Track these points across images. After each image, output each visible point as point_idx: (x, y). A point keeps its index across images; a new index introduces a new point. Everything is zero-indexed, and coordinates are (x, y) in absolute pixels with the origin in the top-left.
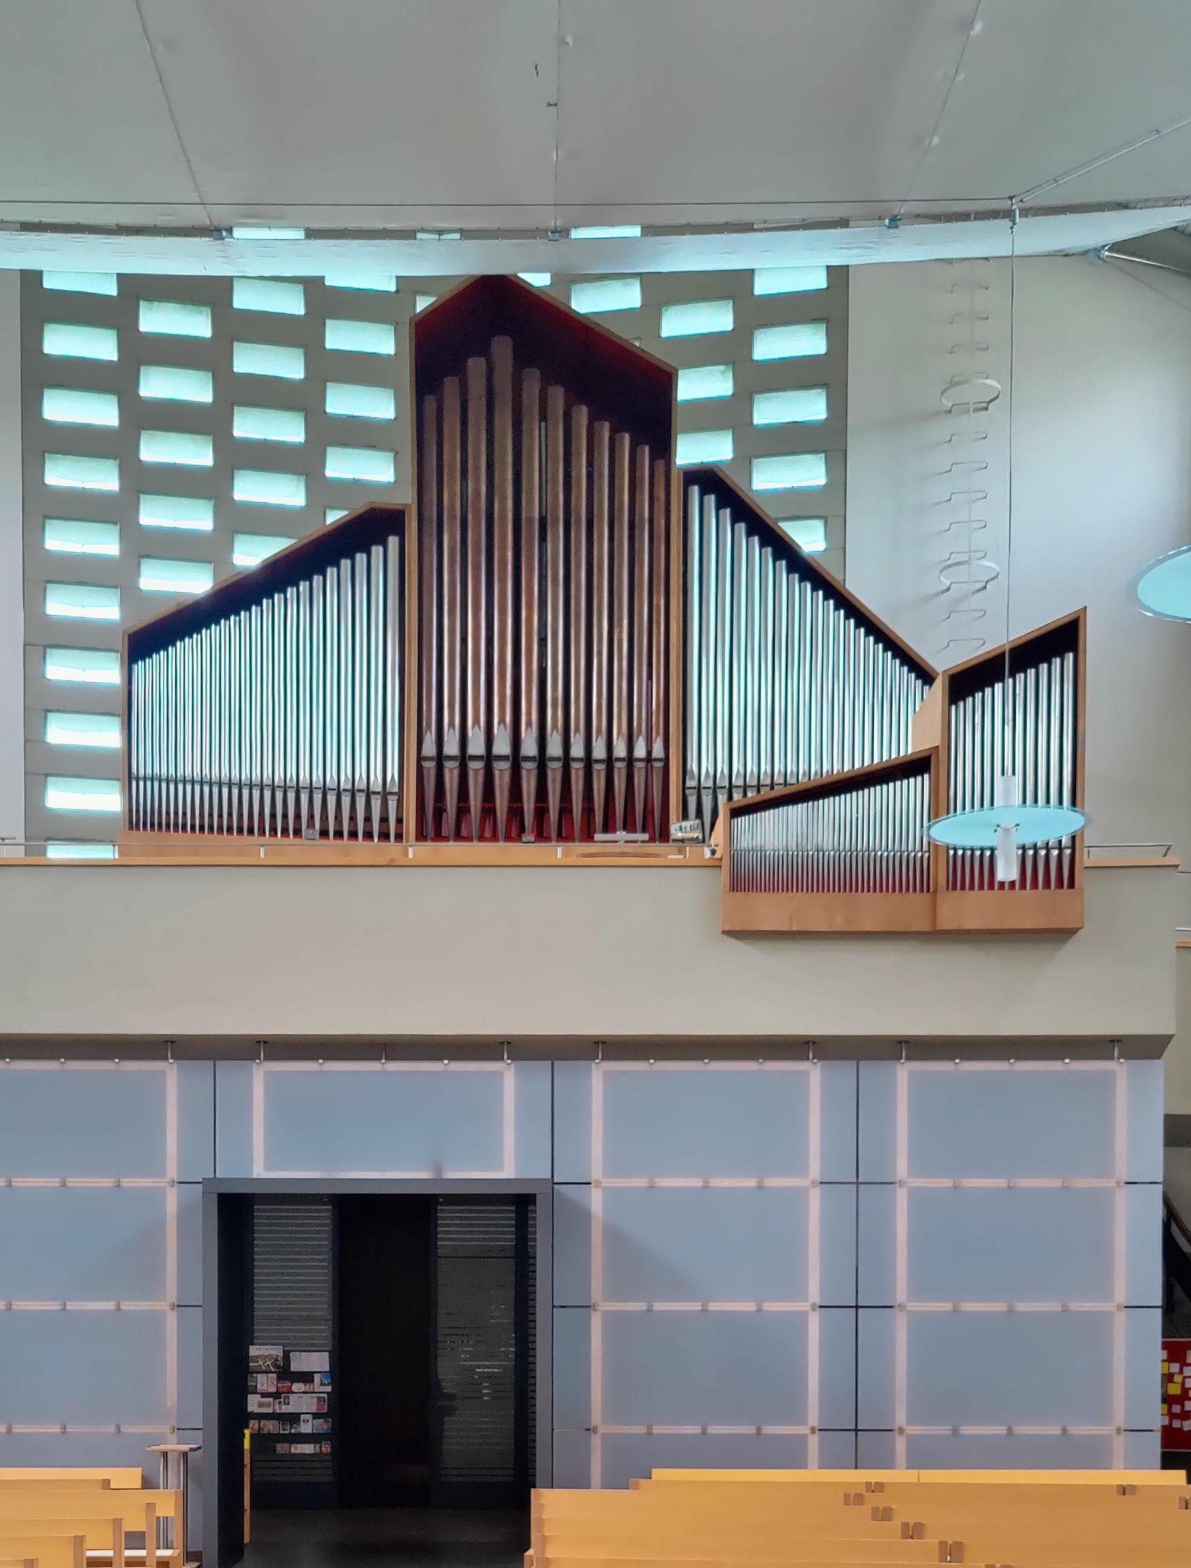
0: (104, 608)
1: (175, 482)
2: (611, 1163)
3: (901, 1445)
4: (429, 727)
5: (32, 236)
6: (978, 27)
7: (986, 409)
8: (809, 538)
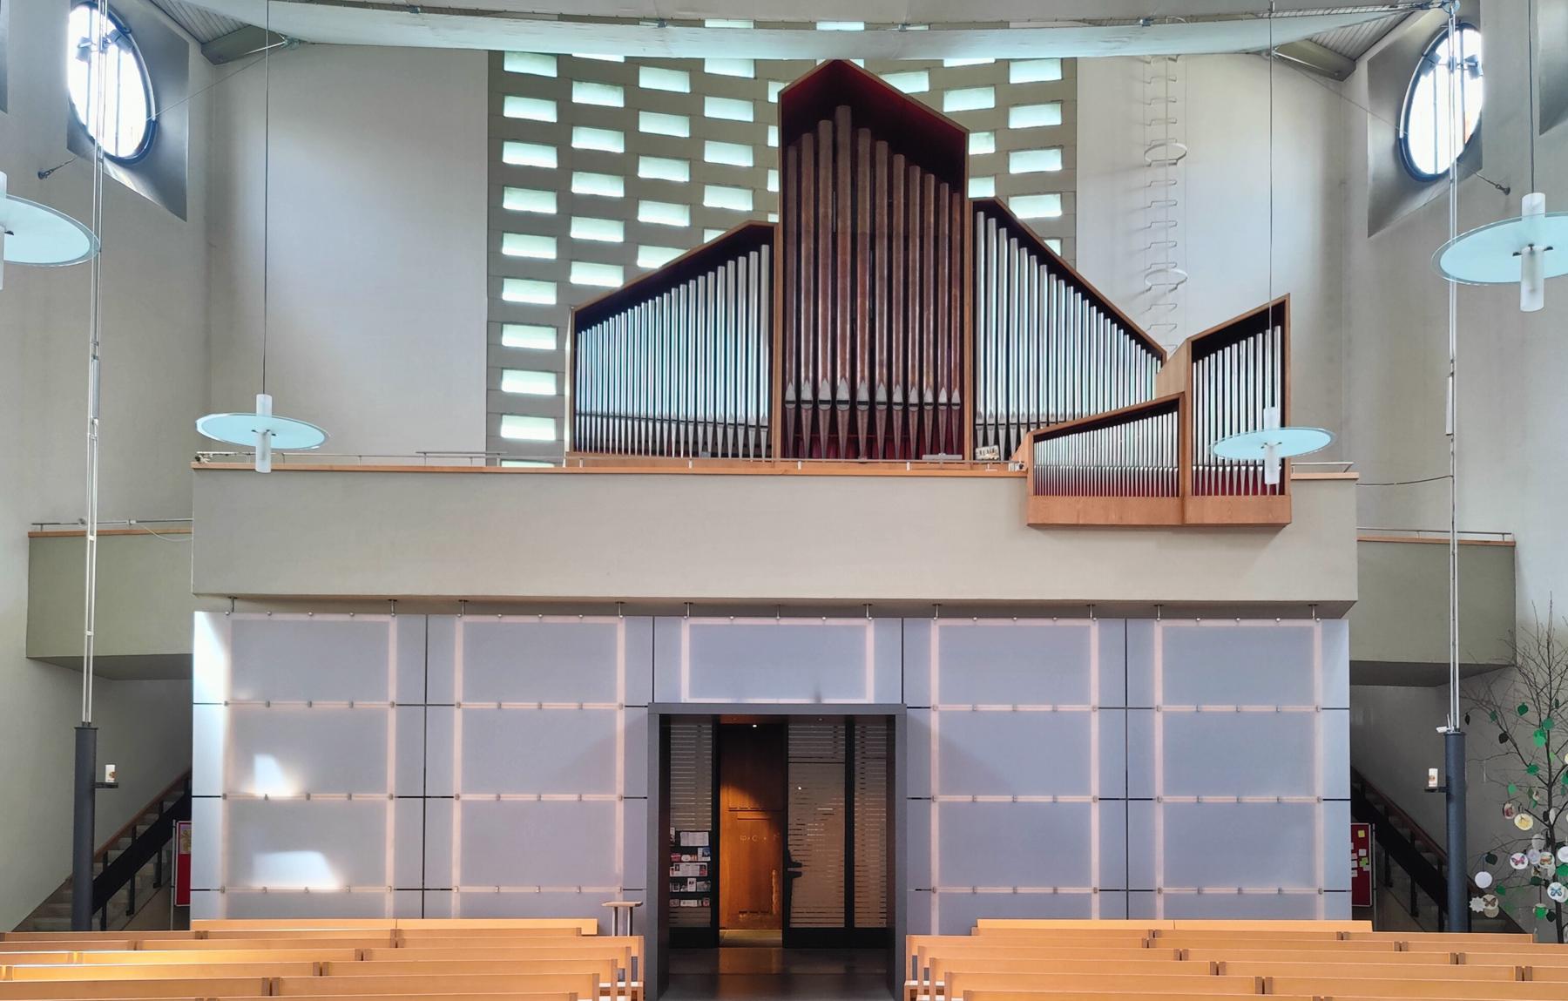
0: (543, 295)
1: (596, 207)
2: (940, 689)
3: (1160, 902)
8: (1055, 246)
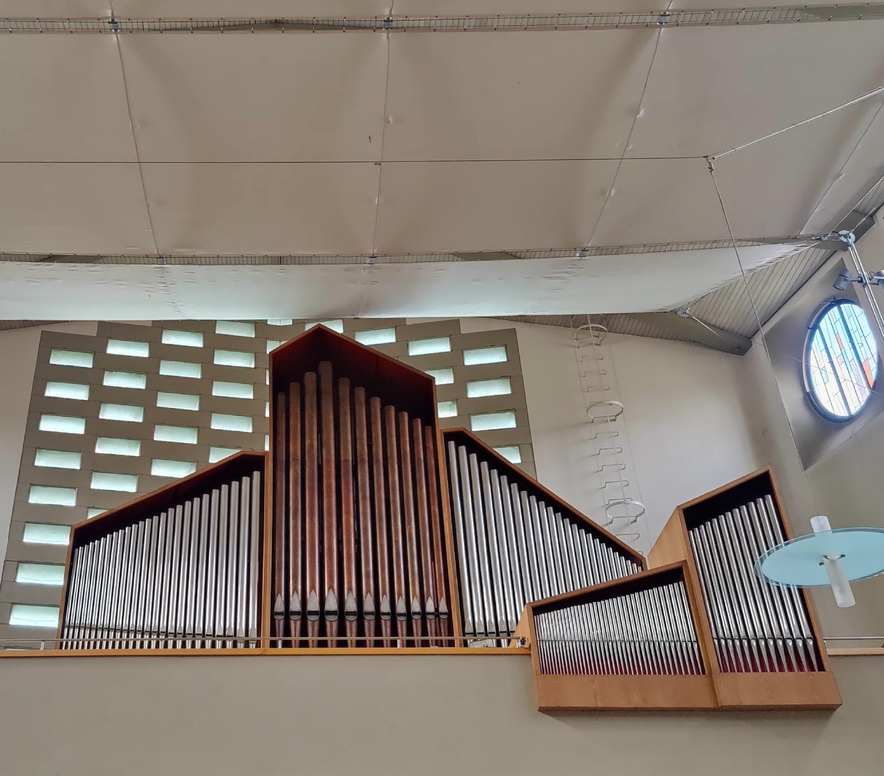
4: (280, 592)
5: (44, 266)
6: (642, 112)
7: (615, 420)
8: (513, 457)
